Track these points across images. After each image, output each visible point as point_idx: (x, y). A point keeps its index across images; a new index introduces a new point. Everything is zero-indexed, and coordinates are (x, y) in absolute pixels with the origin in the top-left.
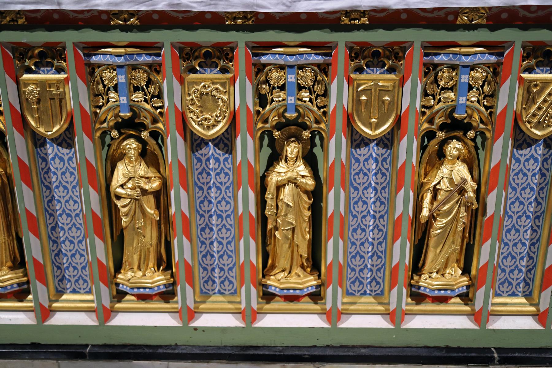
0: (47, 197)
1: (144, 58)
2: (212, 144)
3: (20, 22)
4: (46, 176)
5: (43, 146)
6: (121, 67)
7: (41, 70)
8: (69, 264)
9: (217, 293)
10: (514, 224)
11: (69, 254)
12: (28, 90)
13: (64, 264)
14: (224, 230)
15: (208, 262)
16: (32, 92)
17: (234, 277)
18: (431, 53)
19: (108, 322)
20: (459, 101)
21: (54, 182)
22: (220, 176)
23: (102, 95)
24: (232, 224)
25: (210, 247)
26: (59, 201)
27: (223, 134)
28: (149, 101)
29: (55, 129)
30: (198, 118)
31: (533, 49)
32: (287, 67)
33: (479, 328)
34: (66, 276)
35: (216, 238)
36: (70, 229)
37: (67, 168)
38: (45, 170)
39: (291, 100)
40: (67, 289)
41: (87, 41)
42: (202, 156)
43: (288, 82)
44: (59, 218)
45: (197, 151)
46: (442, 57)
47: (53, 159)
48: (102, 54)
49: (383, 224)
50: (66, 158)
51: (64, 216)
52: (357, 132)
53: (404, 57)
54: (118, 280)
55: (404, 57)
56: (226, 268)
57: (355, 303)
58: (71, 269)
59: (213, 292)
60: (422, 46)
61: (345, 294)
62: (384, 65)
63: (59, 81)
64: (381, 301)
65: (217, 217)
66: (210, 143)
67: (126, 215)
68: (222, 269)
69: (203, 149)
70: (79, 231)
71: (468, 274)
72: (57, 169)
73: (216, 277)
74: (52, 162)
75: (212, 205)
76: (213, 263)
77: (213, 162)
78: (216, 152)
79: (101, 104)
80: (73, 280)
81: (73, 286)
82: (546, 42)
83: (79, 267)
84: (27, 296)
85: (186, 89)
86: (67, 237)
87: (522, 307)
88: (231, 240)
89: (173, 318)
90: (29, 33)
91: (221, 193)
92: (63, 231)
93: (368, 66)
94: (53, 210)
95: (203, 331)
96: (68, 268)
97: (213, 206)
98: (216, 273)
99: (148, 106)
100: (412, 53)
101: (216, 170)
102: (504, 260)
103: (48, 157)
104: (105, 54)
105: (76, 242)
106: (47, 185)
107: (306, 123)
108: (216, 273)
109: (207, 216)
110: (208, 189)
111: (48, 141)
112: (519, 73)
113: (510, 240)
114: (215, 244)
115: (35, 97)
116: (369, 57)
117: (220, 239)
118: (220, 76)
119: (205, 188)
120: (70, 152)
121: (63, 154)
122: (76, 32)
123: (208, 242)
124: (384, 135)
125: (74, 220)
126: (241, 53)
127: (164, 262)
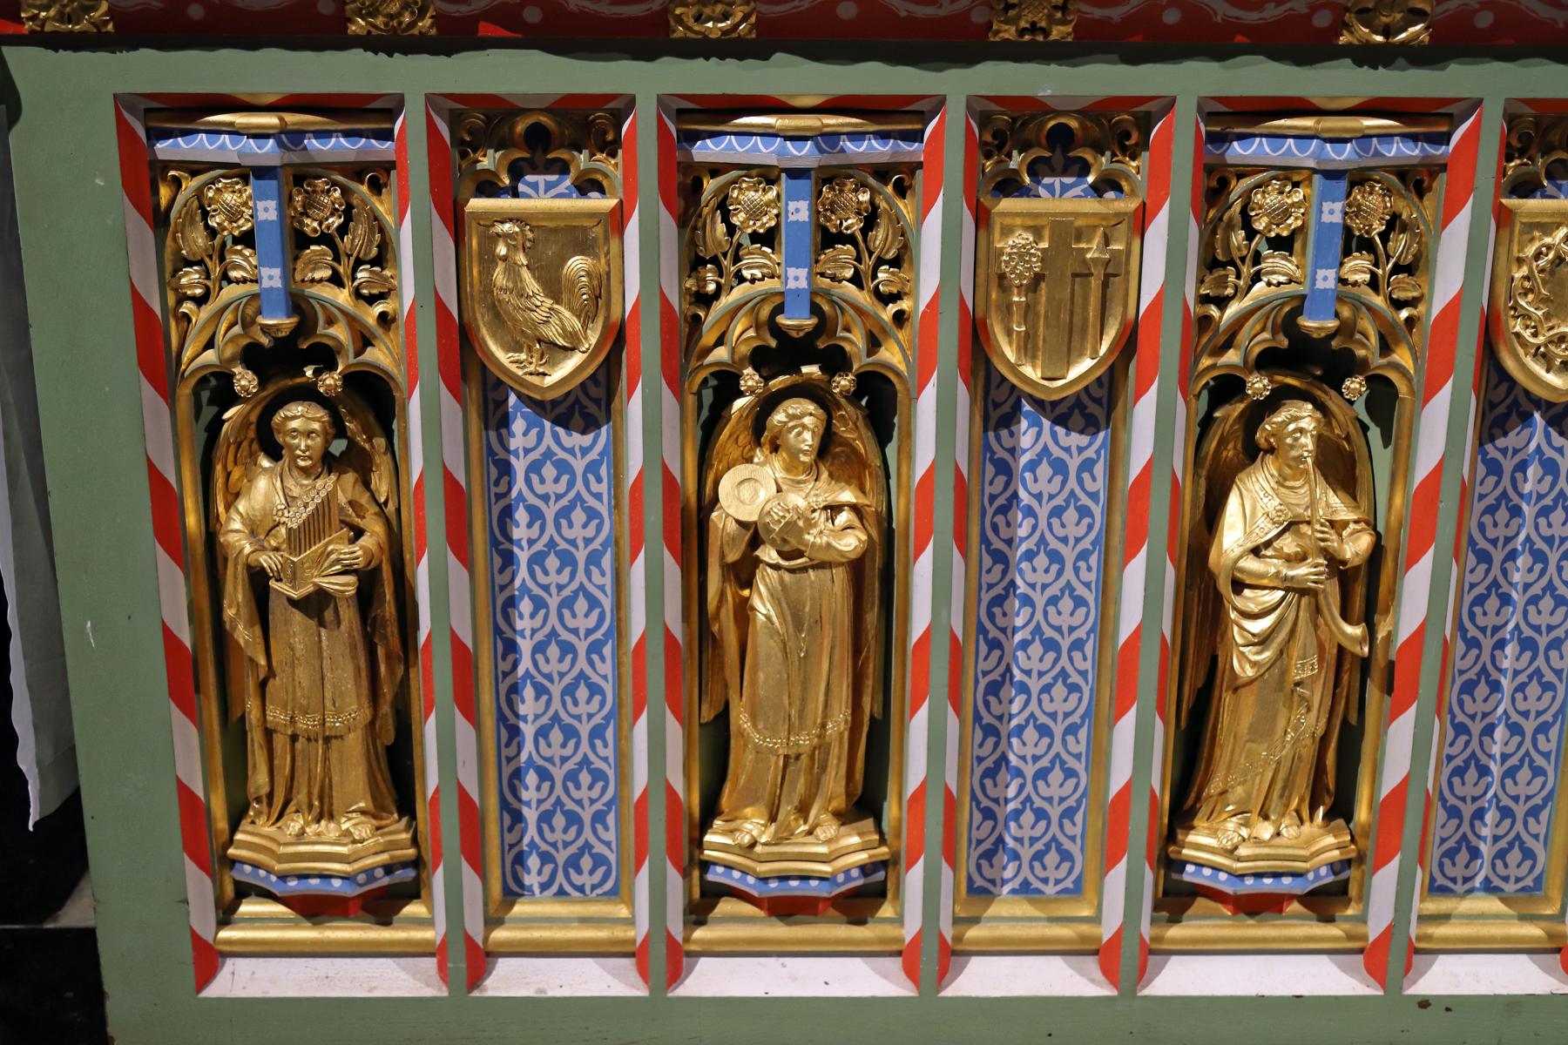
0: (990, 586)
1: (1398, 147)
2: (1542, 416)
3: (1057, 33)
4: (1000, 519)
5: (1008, 426)
6: (262, 172)
7: (529, 184)
8: (1023, 803)
9: (1478, 890)
10: (1484, 665)
11: (1029, 770)
12: (1012, 247)
13: (1007, 801)
14: (1534, 689)
15: (1468, 791)
16: (1022, 254)
17: (1542, 838)
18: (173, 129)
19: (1144, 987)
20: (1314, 280)
21: (1023, 540)
22: (1552, 517)
23: (1238, 262)
24: (1087, 671)
25: (1481, 744)
26: (1027, 601)
27: (583, 385)
28: (1383, 284)
29: (1076, 371)
30: (1535, 335)
31: (1537, 123)
32: (783, 175)
33: (1381, 993)
34: (1008, 839)
35: (1505, 712)
36: (1047, 689)
37: (1072, 493)
38: (1001, 501)
39: (272, 277)
40: (1004, 882)
41: (1245, 94)
42: (1505, 456)
43: (1320, 224)
44: (1020, 654)
45: (1492, 439)
46: (870, 145)
47: (1033, 466)
48: (1267, 136)
49: (1082, 669)
50: (1073, 464)
51: (1036, 649)
52: (1004, 379)
53: (1144, 144)
54: (709, 854)
55: (617, 142)
56: (1520, 810)
57: (1444, 918)
58: (1028, 817)
59: (1468, 886)
60: (1200, 110)
61: (1426, 894)
62: (1084, 169)
63: (488, 219)
64: (1524, 911)
65: (1518, 649)
66: (1537, 416)
67: (1263, 641)
68: (1506, 813)
69: (1512, 434)
70: (1075, 696)
71: (869, 823)
72: (1038, 497)
73: (1484, 839)
74: (1028, 475)
75: (1511, 609)
76: (1482, 791)
77: (1535, 474)
78: (1549, 443)
79: (1230, 291)
80: (1026, 853)
81: (1025, 872)
82: (1048, 102)
83: (1055, 812)
84: (878, 907)
85: (1515, 249)
86: (1032, 715)
87: (526, 929)
88: (1079, 721)
89: (1345, 971)
90: (1064, 69)
91: (1543, 572)
92: (1024, 697)
93: (1550, 177)
94: (1003, 630)
95: (1448, 1009)
96: (1017, 814)
97: (1513, 613)
98: (1485, 825)
99: (1379, 301)
100: (1167, 134)
101: (1540, 497)
102: (1456, 780)
103: (1016, 461)
104: (215, 131)
105: (1058, 730)
106: (997, 550)
107: (842, 349)
108: (1485, 825)
109: (1487, 643)
110: (1505, 560)
111: (1027, 407)
112: (1496, 196)
113: (1473, 717)
114: (1500, 733)
115: (1030, 269)
116: (1039, 145)
117: (1515, 718)
118: (1092, 205)
119: (1498, 555)
120: (1089, 445)
121: (1067, 450)
122: (1215, 65)
123: (1476, 728)
124: (1086, 389)
125: (1064, 661)
126: (642, 127)
127: (1328, 790)
